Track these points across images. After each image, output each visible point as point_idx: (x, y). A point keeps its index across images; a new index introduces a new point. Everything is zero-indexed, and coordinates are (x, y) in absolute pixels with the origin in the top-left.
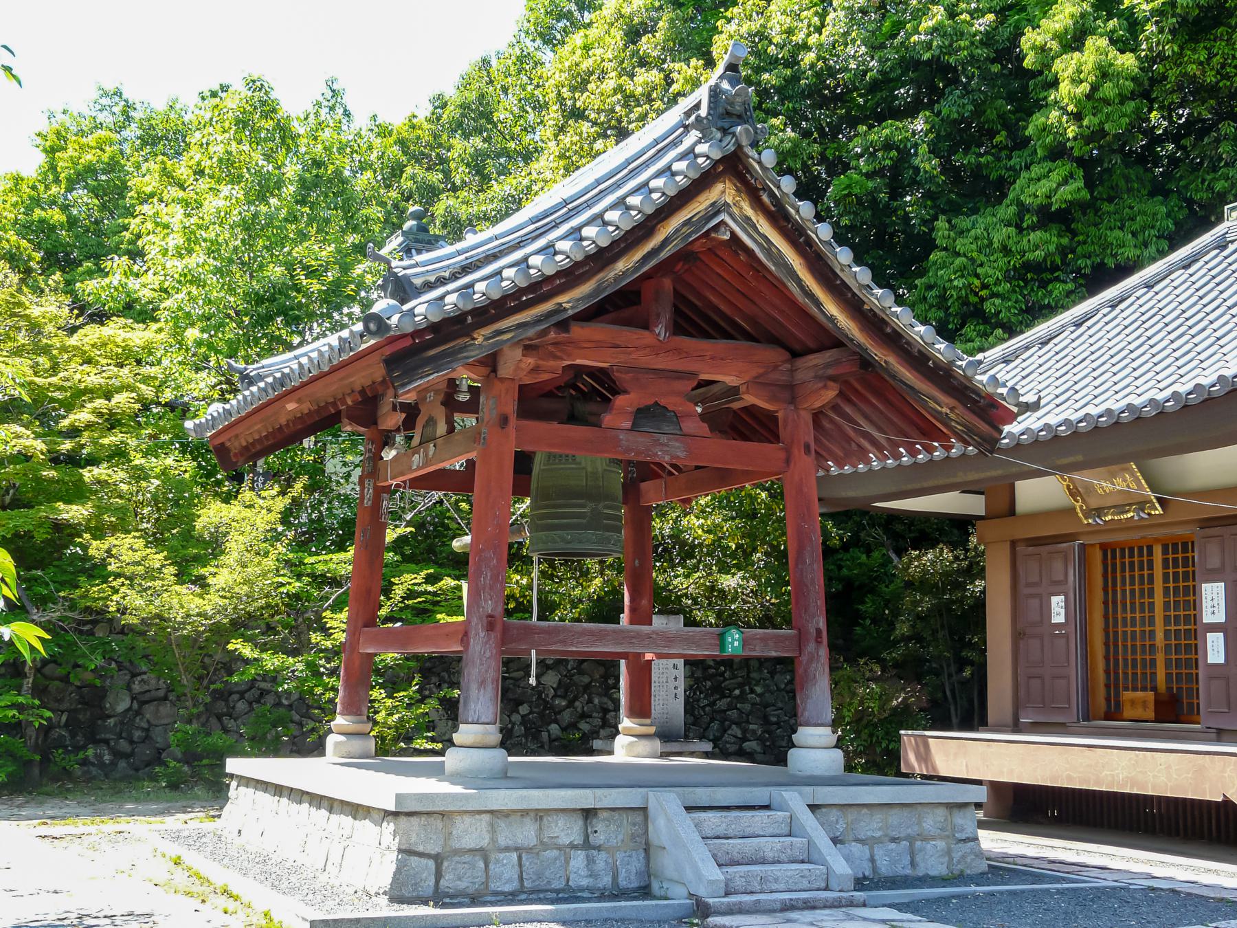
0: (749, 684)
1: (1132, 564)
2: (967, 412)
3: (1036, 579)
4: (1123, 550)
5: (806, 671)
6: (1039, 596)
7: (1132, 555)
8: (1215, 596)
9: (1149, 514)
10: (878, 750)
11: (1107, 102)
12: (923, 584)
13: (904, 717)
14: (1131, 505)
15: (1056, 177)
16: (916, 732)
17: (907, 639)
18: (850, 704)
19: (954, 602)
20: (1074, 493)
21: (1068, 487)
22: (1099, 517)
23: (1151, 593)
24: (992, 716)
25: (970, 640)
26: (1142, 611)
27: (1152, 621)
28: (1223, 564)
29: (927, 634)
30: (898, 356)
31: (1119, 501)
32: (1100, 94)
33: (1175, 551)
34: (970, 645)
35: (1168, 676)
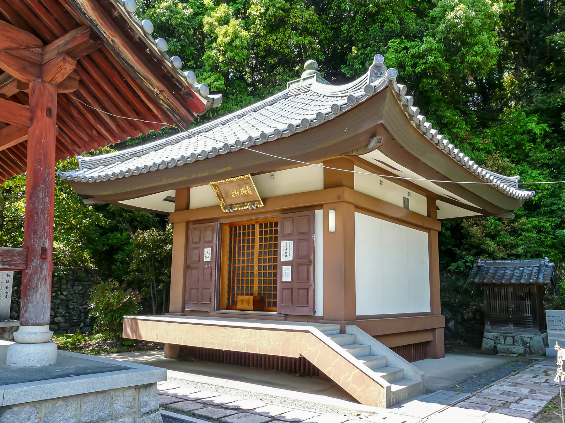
0: (61, 290)
1: (244, 234)
2: (171, 96)
3: (197, 240)
4: (240, 227)
5: (30, 281)
6: (198, 248)
7: (244, 229)
8: (288, 247)
9: (257, 207)
10: (115, 323)
11: (236, 47)
12: (142, 246)
13: (128, 309)
14: (247, 202)
15: (213, 78)
16: (132, 317)
17: (134, 271)
18: (103, 301)
19: (157, 254)
20: (220, 196)
21: (217, 193)
22: (231, 209)
23: (253, 247)
24: (171, 309)
25: (163, 271)
26: (248, 256)
27: (252, 261)
28: (293, 231)
29: (144, 269)
30: (123, 39)
31: (241, 200)
32: (234, 44)
33: (266, 227)
34: (163, 274)
35: (259, 288)
